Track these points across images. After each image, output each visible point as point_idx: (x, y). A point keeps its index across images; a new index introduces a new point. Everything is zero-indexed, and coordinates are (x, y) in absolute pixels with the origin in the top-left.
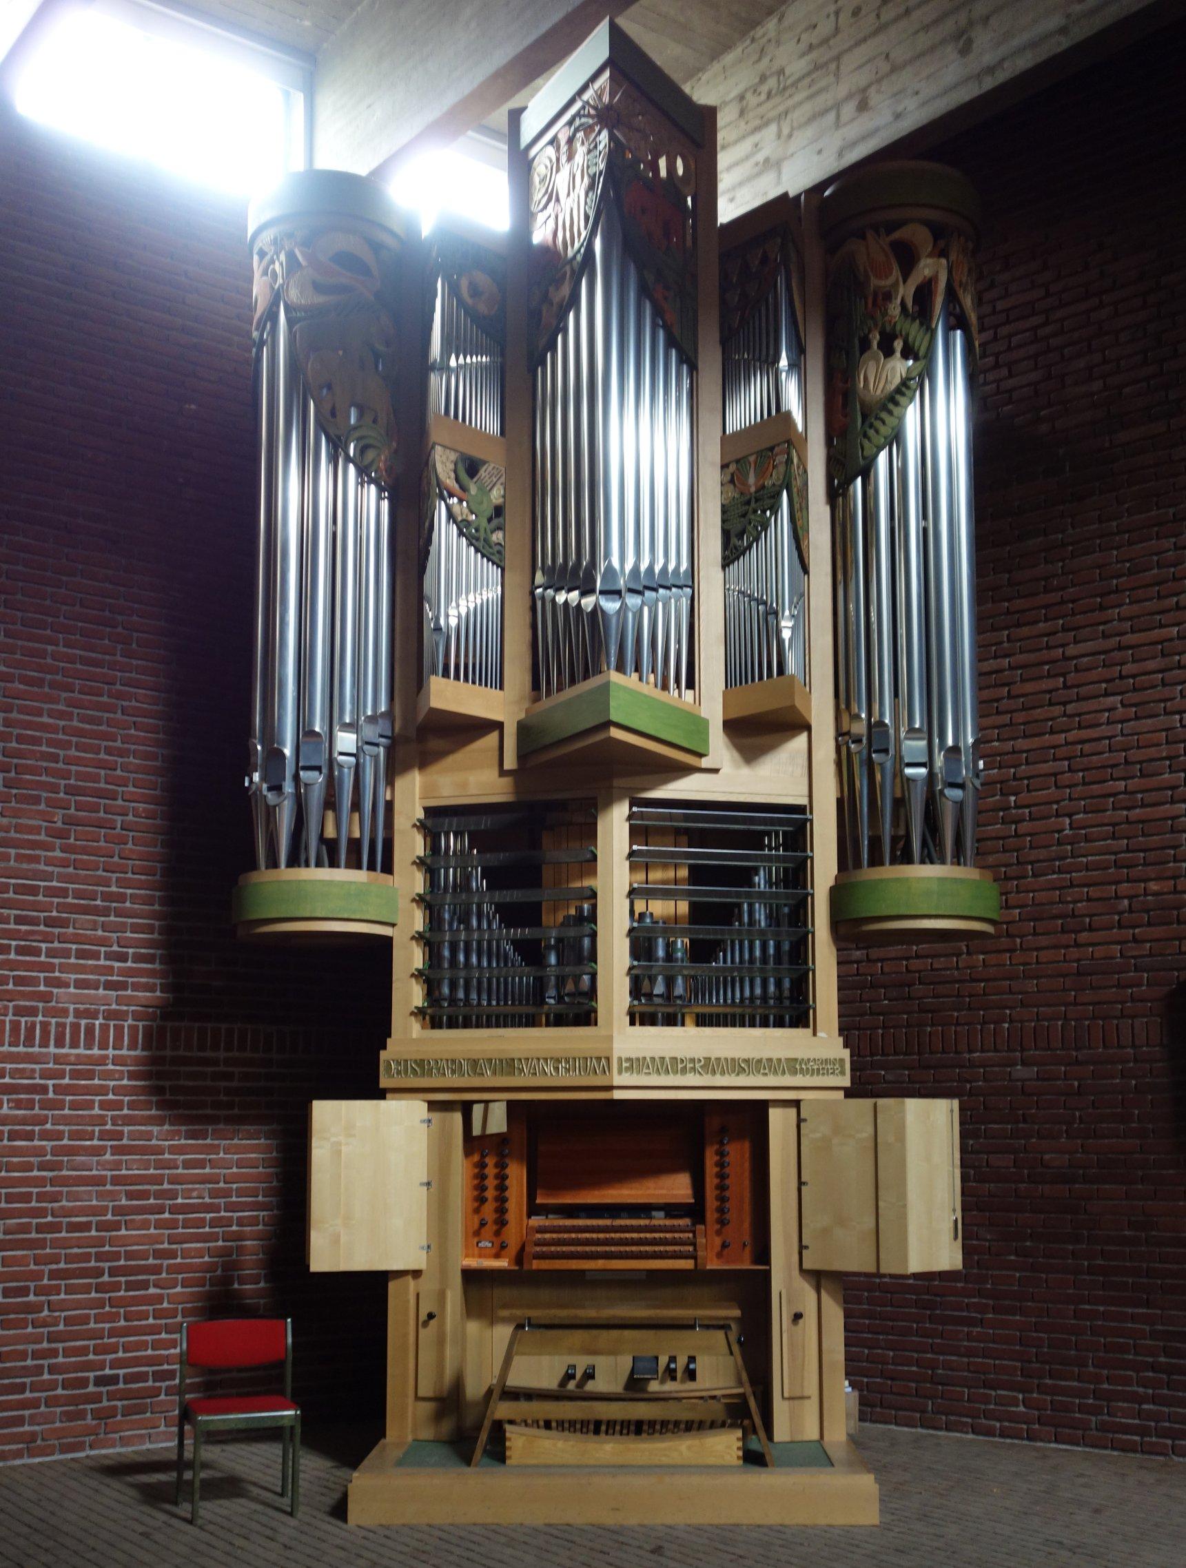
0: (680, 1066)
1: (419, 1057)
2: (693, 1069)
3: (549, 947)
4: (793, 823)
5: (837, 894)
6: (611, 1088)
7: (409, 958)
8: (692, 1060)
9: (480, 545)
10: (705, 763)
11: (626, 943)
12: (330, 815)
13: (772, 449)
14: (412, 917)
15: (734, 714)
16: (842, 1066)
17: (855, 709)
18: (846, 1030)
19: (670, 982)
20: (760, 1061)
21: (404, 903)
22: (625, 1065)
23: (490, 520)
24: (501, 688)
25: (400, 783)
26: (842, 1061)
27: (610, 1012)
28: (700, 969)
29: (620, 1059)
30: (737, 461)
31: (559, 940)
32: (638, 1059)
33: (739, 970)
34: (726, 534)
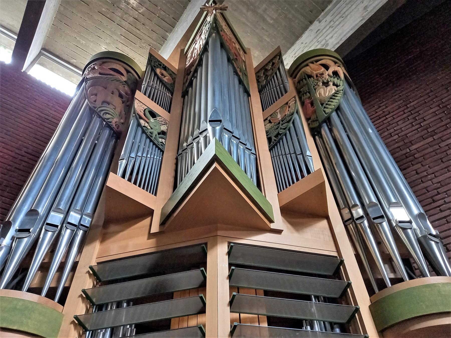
9: (153, 139)
10: (272, 226)
11: (227, 283)
13: (287, 103)
15: (285, 202)
17: (351, 203)
24: (155, 195)
25: (86, 249)
30: (271, 116)
34: (269, 140)
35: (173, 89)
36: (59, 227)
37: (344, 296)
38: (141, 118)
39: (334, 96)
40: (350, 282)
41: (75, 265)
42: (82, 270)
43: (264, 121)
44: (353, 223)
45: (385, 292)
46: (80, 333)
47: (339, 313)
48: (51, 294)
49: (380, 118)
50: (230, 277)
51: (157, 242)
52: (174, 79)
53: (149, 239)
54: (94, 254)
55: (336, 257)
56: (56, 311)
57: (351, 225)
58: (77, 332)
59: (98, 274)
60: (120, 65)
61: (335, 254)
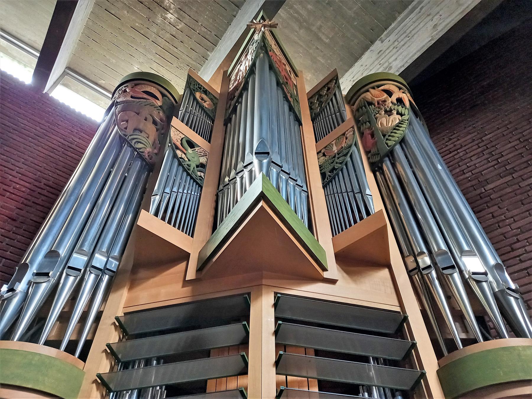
5: (442, 375)
10: (326, 275)
11: (272, 340)
13: (344, 134)
17: (417, 250)
23: (197, 166)
24: (192, 236)
25: (112, 297)
30: (325, 148)
34: (323, 175)
35: (215, 116)
37: (409, 358)
38: (177, 148)
39: (398, 126)
40: (414, 342)
41: (99, 316)
42: (107, 320)
43: (318, 153)
48: (71, 348)
49: (451, 153)
50: (276, 333)
51: (193, 291)
52: (215, 104)
53: (183, 287)
54: (121, 303)
55: (399, 312)
57: (416, 276)
60: (154, 87)
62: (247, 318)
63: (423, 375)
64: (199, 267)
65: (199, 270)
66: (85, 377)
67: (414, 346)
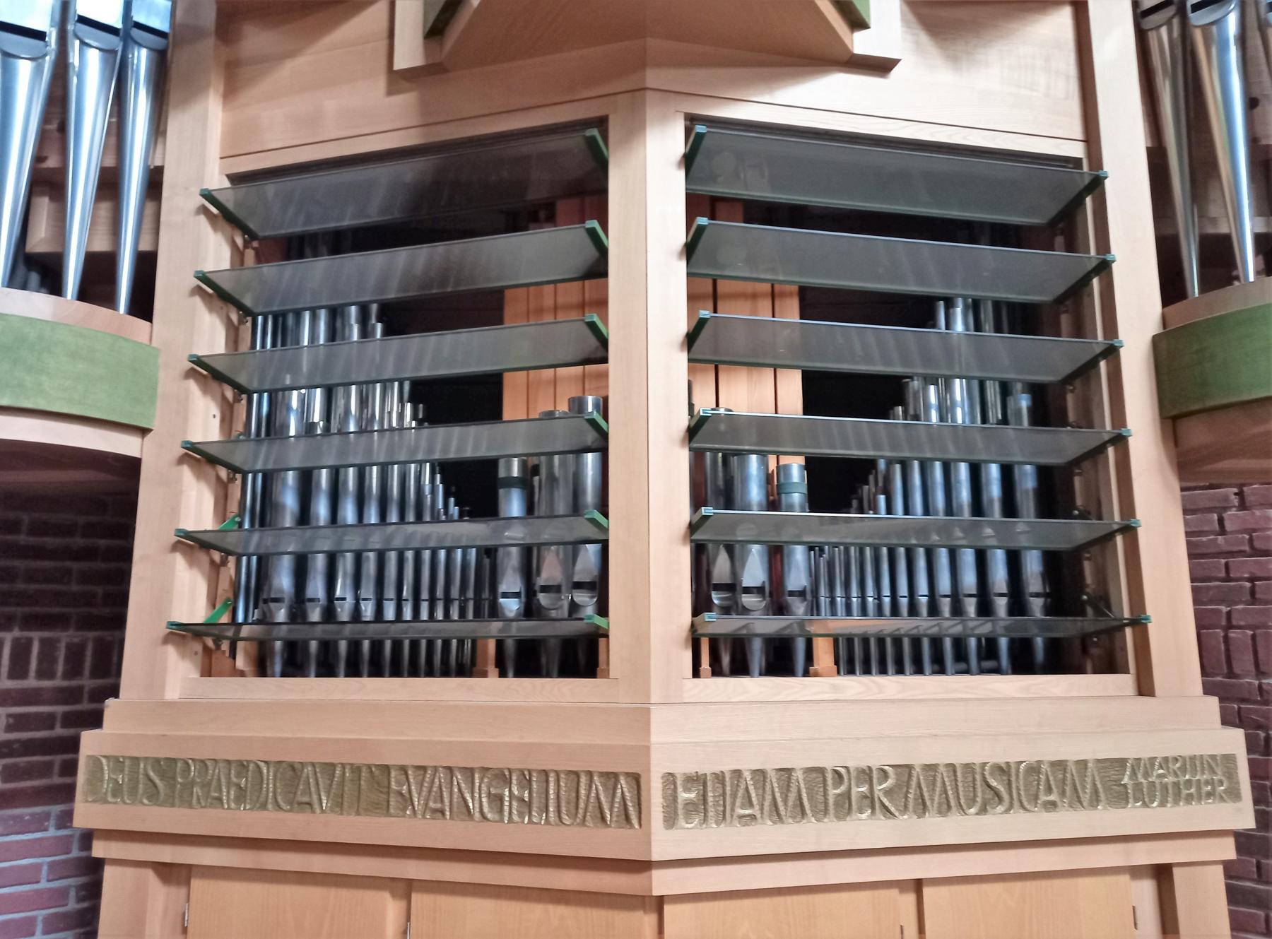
0: (833, 792)
1: (163, 753)
2: (870, 800)
3: (510, 483)
4: (1060, 203)
5: (1166, 351)
6: (644, 866)
7: (179, 503)
8: (866, 775)
10: (861, 44)
11: (682, 459)
12: (44, 205)
14: (183, 413)
16: (1231, 774)
18: (1218, 671)
19: (776, 555)
20: (1034, 769)
21: (170, 377)
22: (683, 796)
25: (176, 123)
26: (1229, 759)
27: (642, 639)
28: (847, 527)
29: (670, 779)
31: (530, 471)
32: (720, 778)
33: (944, 529)
36: (52, 38)
37: (1075, 304)
40: (1109, 257)
41: (154, 183)
42: (180, 201)
44: (1176, 22)
45: (1228, 301)
46: (224, 398)
47: (1050, 356)
48: (97, 284)
50: (690, 250)
51: (425, 106)
53: (391, 92)
54: (205, 145)
55: (1077, 162)
56: (126, 340)
57: (1164, 31)
58: (214, 398)
59: (240, 214)
61: (1076, 150)
62: (605, 274)
63: (1111, 352)
64: (429, 25)
65: (435, 31)
66: (161, 360)
67: (1104, 268)
